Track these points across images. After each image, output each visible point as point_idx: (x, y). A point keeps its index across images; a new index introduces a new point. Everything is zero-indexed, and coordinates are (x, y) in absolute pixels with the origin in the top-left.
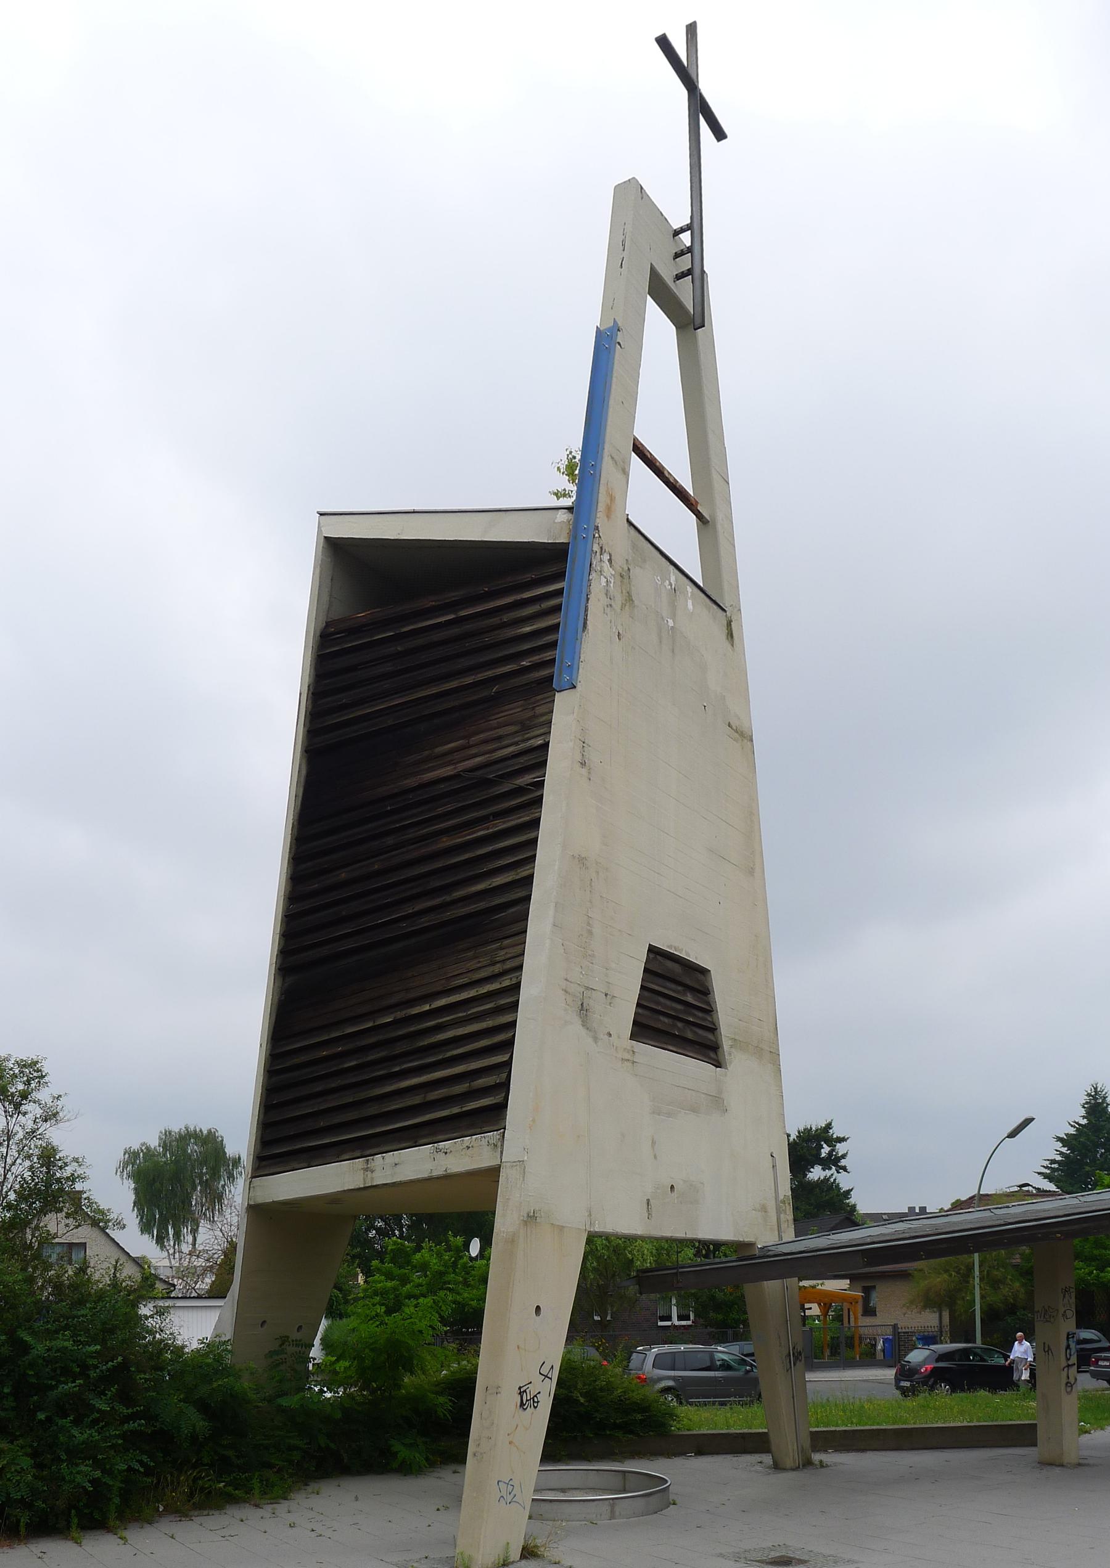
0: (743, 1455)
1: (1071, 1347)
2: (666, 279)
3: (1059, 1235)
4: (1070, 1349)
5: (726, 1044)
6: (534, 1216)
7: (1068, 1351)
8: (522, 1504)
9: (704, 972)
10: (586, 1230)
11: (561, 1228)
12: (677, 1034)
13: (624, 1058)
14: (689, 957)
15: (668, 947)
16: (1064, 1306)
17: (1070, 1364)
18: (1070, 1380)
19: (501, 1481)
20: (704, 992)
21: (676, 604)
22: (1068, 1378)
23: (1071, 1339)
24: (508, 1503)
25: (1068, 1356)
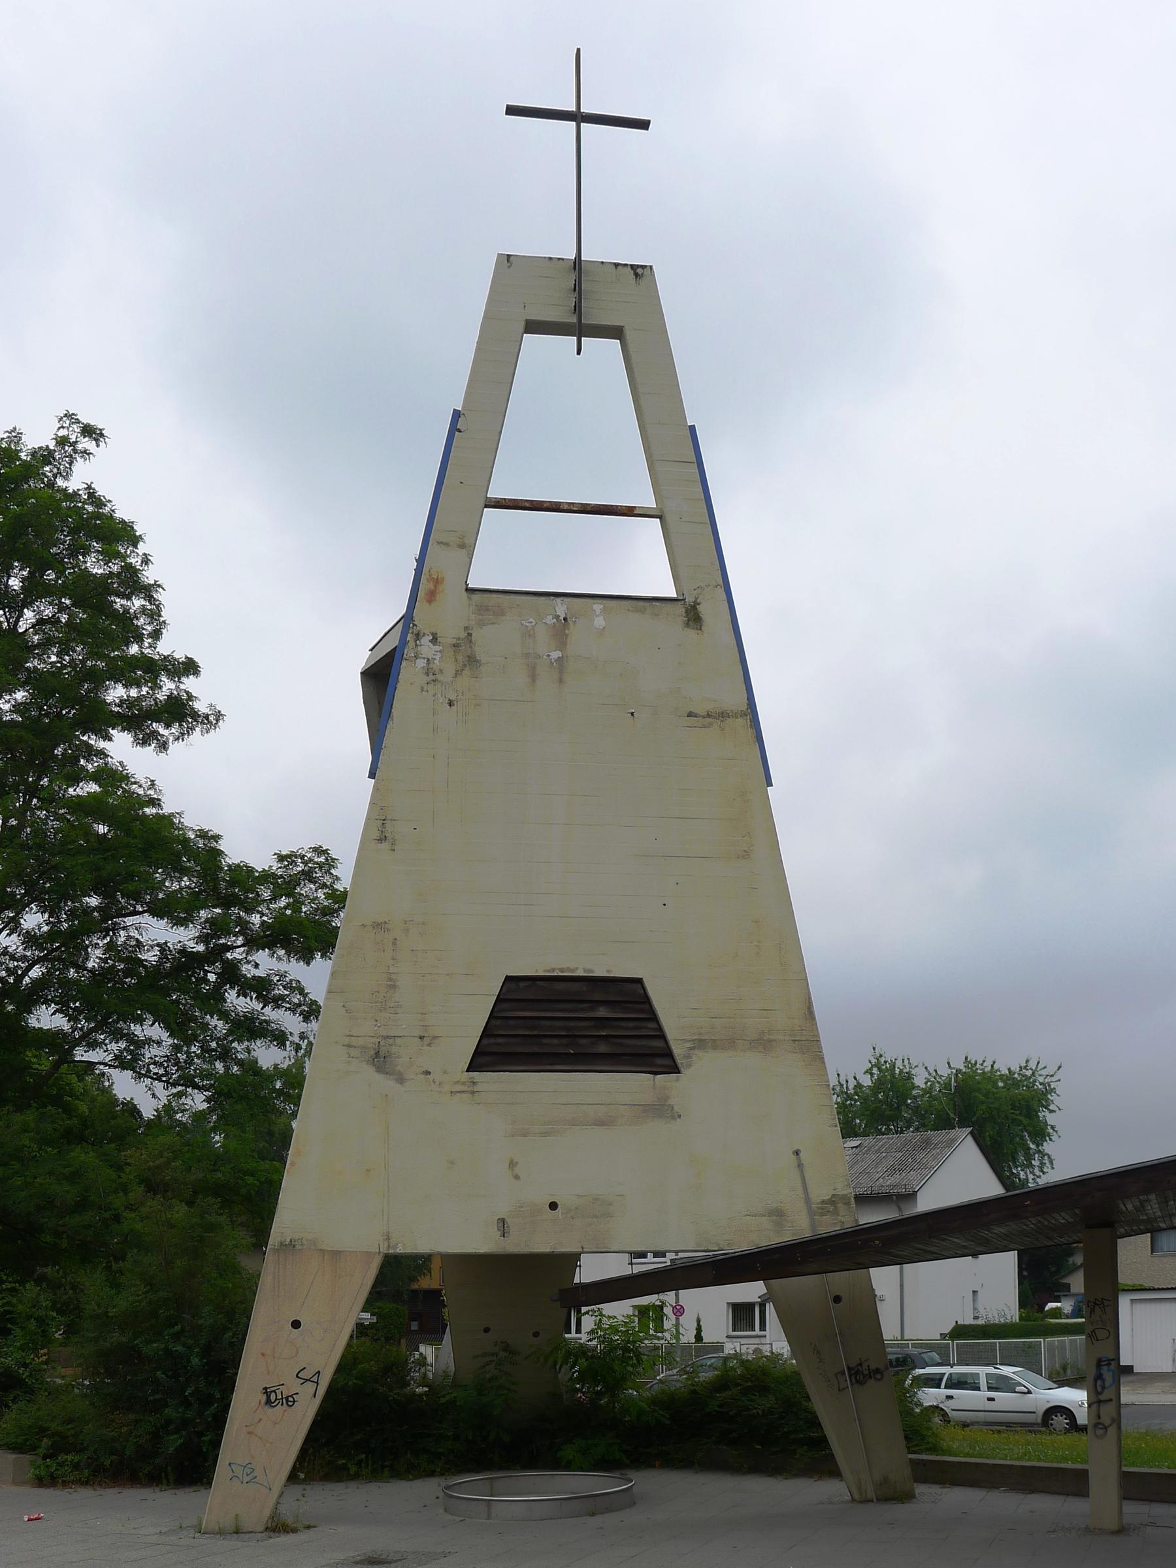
0: (645, 1481)
1: (1104, 1377)
2: (567, 321)
3: (878, 1242)
4: (1103, 1381)
5: (677, 1050)
6: (291, 1244)
7: (1099, 1382)
8: (268, 1486)
9: (639, 981)
10: (379, 1252)
11: (336, 1254)
12: (572, 1052)
13: (453, 1090)
14: (592, 972)
15: (545, 971)
16: (1092, 1324)
17: (1102, 1399)
18: (1101, 1421)
19: (233, 1463)
20: (646, 1000)
21: (567, 631)
22: (1099, 1417)
23: (1105, 1368)
24: (245, 1482)
25: (1099, 1389)
